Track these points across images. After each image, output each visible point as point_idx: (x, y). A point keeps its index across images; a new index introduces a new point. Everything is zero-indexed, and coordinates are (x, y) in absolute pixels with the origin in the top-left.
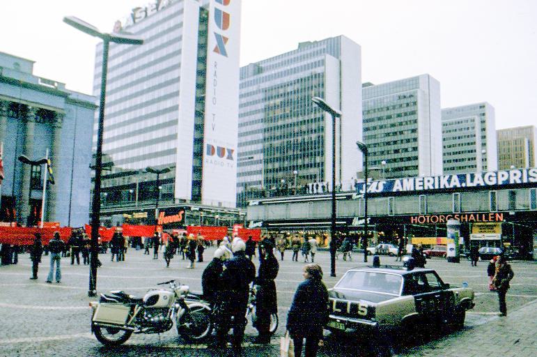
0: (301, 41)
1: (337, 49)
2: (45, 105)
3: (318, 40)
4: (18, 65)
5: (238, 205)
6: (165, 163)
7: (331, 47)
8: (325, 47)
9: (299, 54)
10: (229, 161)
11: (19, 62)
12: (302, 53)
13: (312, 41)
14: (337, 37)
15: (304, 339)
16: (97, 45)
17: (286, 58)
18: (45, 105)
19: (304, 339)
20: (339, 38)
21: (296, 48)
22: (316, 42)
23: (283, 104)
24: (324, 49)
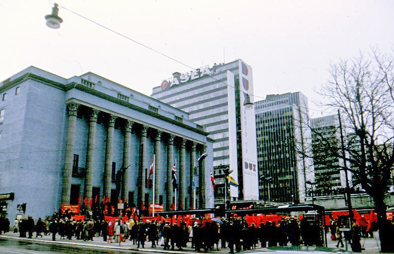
0: (268, 94)
1: (297, 97)
2: (153, 125)
3: (280, 94)
4: (100, 82)
5: (260, 198)
6: (102, 91)
7: (292, 98)
8: (288, 98)
9: (267, 103)
10: (254, 172)
11: (101, 80)
12: (269, 103)
13: (275, 94)
14: (296, 93)
15: (219, 232)
16: (154, 88)
17: (260, 105)
18: (153, 125)
19: (219, 232)
20: (297, 93)
21: (264, 98)
22: (278, 95)
23: (291, 151)
24: (287, 100)
